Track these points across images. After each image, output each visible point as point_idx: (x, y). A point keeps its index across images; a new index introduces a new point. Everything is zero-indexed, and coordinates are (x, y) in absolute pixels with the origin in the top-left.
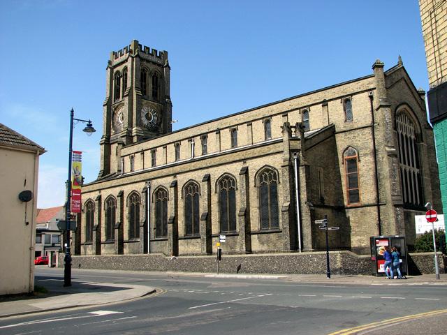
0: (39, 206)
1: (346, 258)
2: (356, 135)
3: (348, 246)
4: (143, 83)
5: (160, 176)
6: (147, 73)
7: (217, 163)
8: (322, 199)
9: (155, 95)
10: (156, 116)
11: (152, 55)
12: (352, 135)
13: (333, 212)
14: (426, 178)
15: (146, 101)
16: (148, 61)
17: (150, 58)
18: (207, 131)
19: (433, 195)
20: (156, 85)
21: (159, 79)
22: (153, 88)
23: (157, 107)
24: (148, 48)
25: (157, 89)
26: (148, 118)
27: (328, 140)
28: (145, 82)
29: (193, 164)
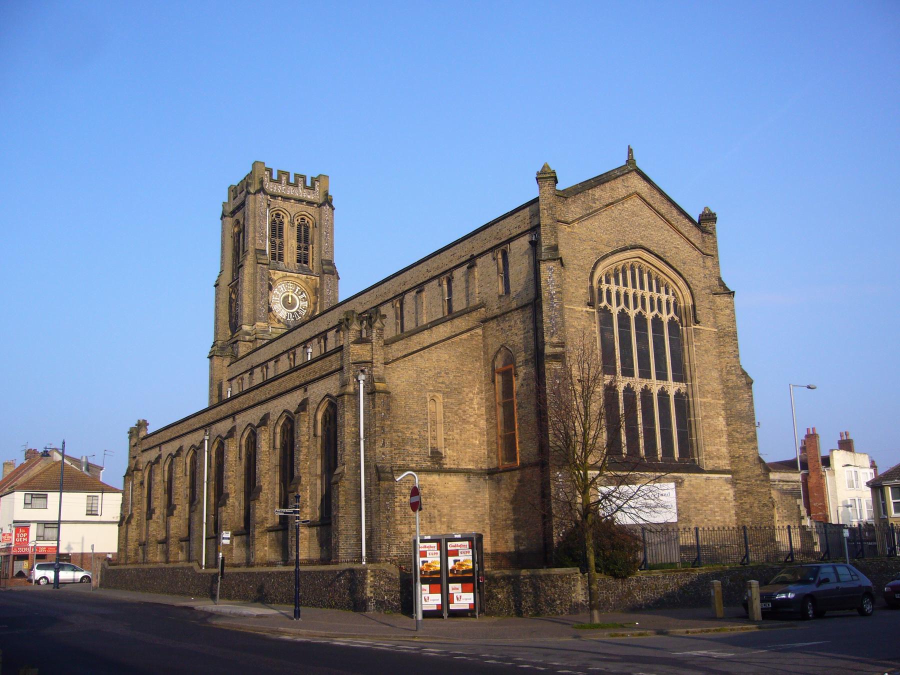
0: (867, 456)
1: (381, 579)
2: (513, 323)
3: (80, 558)
4: (278, 241)
5: (218, 417)
6: (286, 221)
7: (272, 394)
8: (436, 456)
9: (303, 259)
10: (305, 299)
11: (296, 185)
12: (507, 324)
13: (469, 481)
14: (709, 399)
15: (281, 274)
16: (286, 198)
17: (291, 191)
18: (326, 327)
19: (730, 435)
20: (306, 241)
21: (311, 230)
22: (299, 248)
23: (307, 283)
24: (304, 177)
25: (306, 249)
26: (288, 304)
27: (464, 336)
28: (281, 236)
29: (252, 394)
